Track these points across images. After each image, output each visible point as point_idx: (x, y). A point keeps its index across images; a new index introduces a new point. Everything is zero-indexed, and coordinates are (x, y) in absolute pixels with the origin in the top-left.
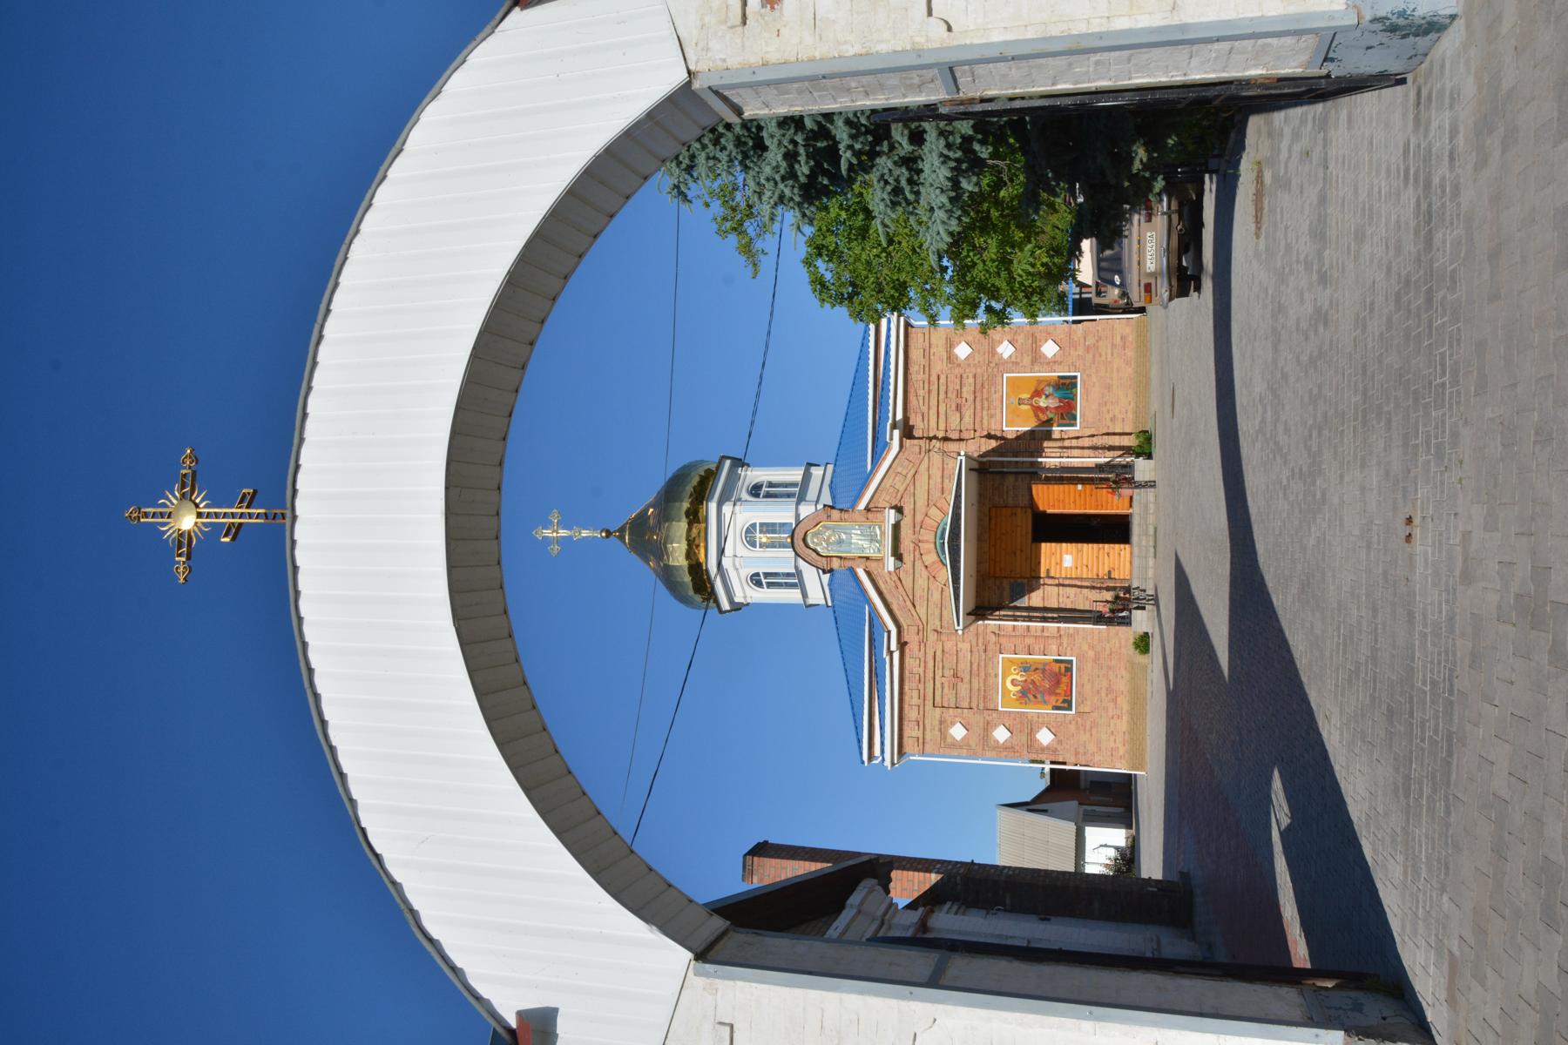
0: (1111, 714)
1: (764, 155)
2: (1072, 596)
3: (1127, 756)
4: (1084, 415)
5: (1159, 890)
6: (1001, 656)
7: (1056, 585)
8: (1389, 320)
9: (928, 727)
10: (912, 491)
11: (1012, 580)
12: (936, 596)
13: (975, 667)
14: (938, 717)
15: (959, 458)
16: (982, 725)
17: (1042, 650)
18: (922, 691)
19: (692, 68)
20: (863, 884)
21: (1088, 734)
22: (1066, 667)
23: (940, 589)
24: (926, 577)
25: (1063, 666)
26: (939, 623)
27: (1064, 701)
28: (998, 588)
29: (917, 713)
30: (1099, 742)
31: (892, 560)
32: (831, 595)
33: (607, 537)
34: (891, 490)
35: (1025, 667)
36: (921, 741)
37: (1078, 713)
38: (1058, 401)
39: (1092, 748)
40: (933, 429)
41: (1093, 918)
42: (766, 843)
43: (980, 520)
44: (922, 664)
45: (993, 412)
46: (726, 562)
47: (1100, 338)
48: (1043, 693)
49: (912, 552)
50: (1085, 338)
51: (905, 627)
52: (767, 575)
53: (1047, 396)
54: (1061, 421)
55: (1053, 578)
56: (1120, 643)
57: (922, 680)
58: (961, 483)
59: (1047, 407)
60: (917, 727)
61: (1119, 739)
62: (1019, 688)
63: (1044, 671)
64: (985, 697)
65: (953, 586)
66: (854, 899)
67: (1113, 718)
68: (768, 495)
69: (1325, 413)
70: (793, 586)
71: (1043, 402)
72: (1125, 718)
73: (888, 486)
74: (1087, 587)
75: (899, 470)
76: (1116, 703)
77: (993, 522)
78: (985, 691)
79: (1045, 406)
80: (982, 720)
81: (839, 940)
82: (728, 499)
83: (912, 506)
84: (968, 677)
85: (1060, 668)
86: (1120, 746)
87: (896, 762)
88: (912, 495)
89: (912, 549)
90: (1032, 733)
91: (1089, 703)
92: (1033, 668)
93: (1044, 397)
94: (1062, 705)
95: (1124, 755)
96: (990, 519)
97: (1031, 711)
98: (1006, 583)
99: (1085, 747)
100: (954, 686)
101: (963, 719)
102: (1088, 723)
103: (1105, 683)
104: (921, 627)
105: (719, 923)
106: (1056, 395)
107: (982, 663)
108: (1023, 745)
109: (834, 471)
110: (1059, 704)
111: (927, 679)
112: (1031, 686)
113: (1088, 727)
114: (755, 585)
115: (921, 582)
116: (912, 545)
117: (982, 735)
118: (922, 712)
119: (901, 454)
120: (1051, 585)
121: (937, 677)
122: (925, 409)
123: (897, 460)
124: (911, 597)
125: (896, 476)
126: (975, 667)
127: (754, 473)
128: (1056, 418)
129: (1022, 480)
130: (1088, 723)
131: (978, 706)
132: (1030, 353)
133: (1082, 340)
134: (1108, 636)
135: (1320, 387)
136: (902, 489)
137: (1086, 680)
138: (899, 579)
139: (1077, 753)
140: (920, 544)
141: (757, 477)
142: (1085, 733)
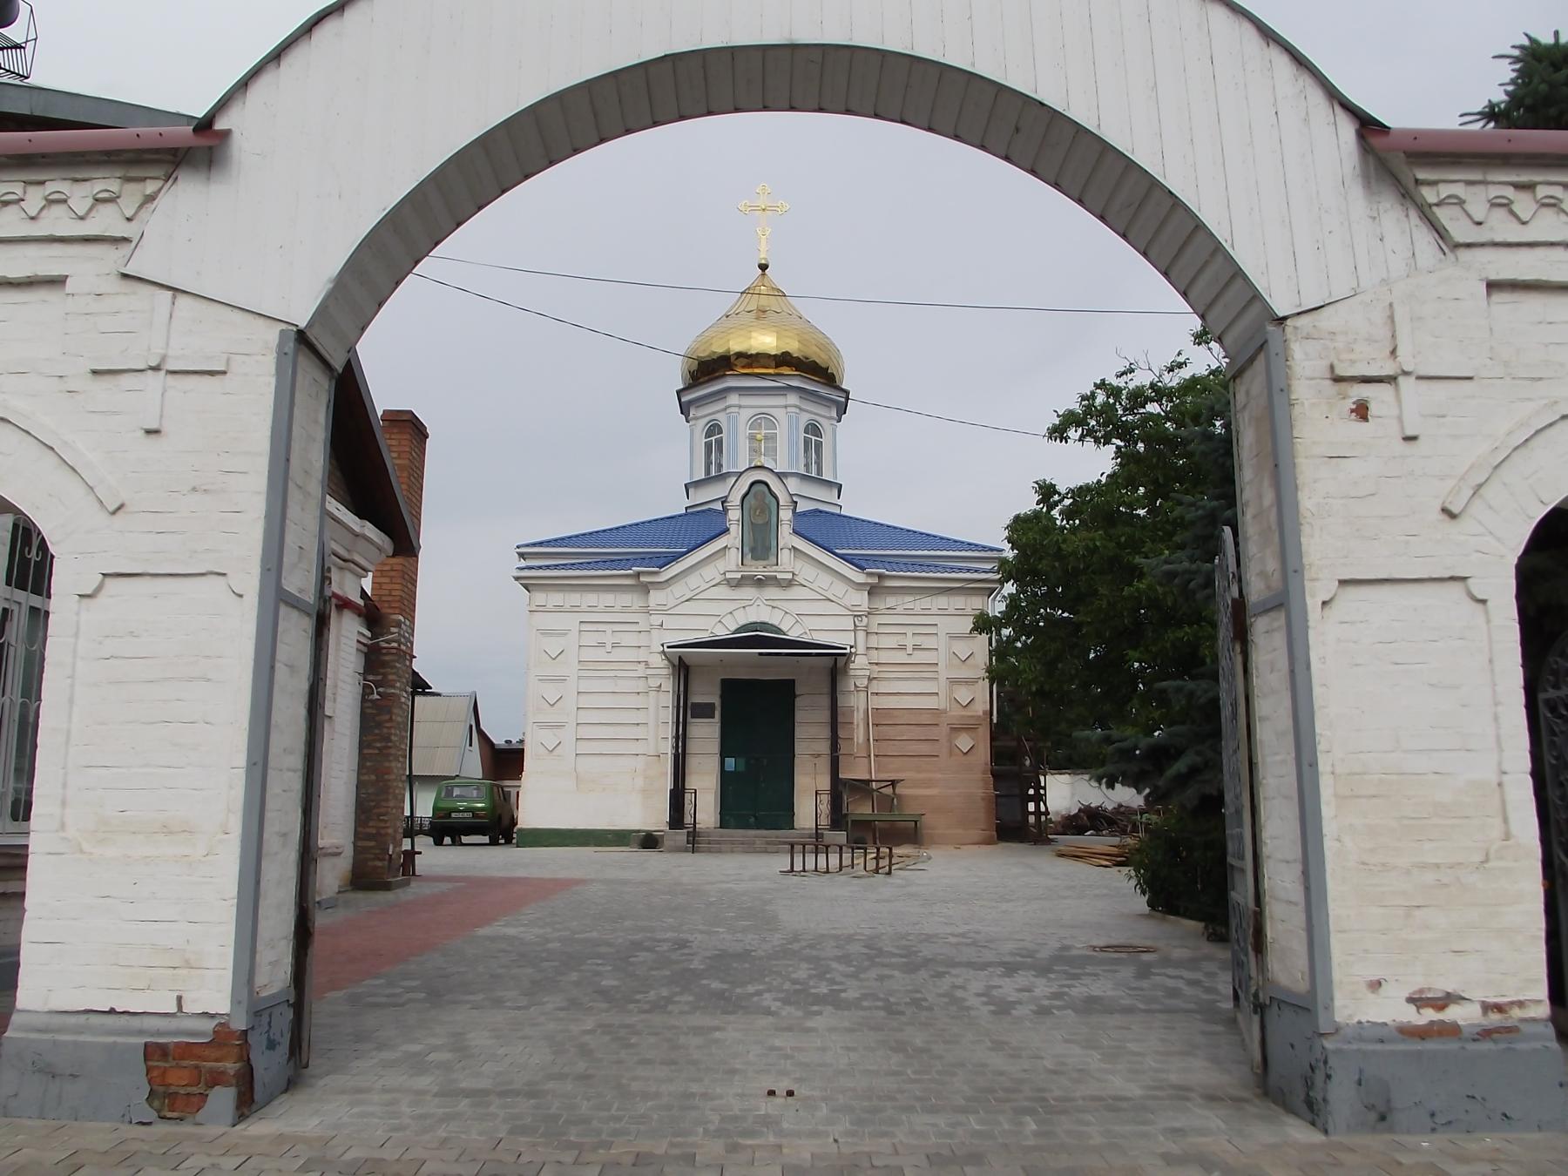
1: (1206, 373)
5: (391, 856)
8: (1001, 1073)
15: (848, 647)
19: (1289, 322)
20: (387, 539)
32: (698, 512)
41: (359, 774)
42: (426, 436)
52: (720, 442)
66: (370, 530)
68: (807, 442)
69: (902, 1013)
81: (325, 513)
105: (339, 366)
109: (833, 514)
135: (930, 1009)
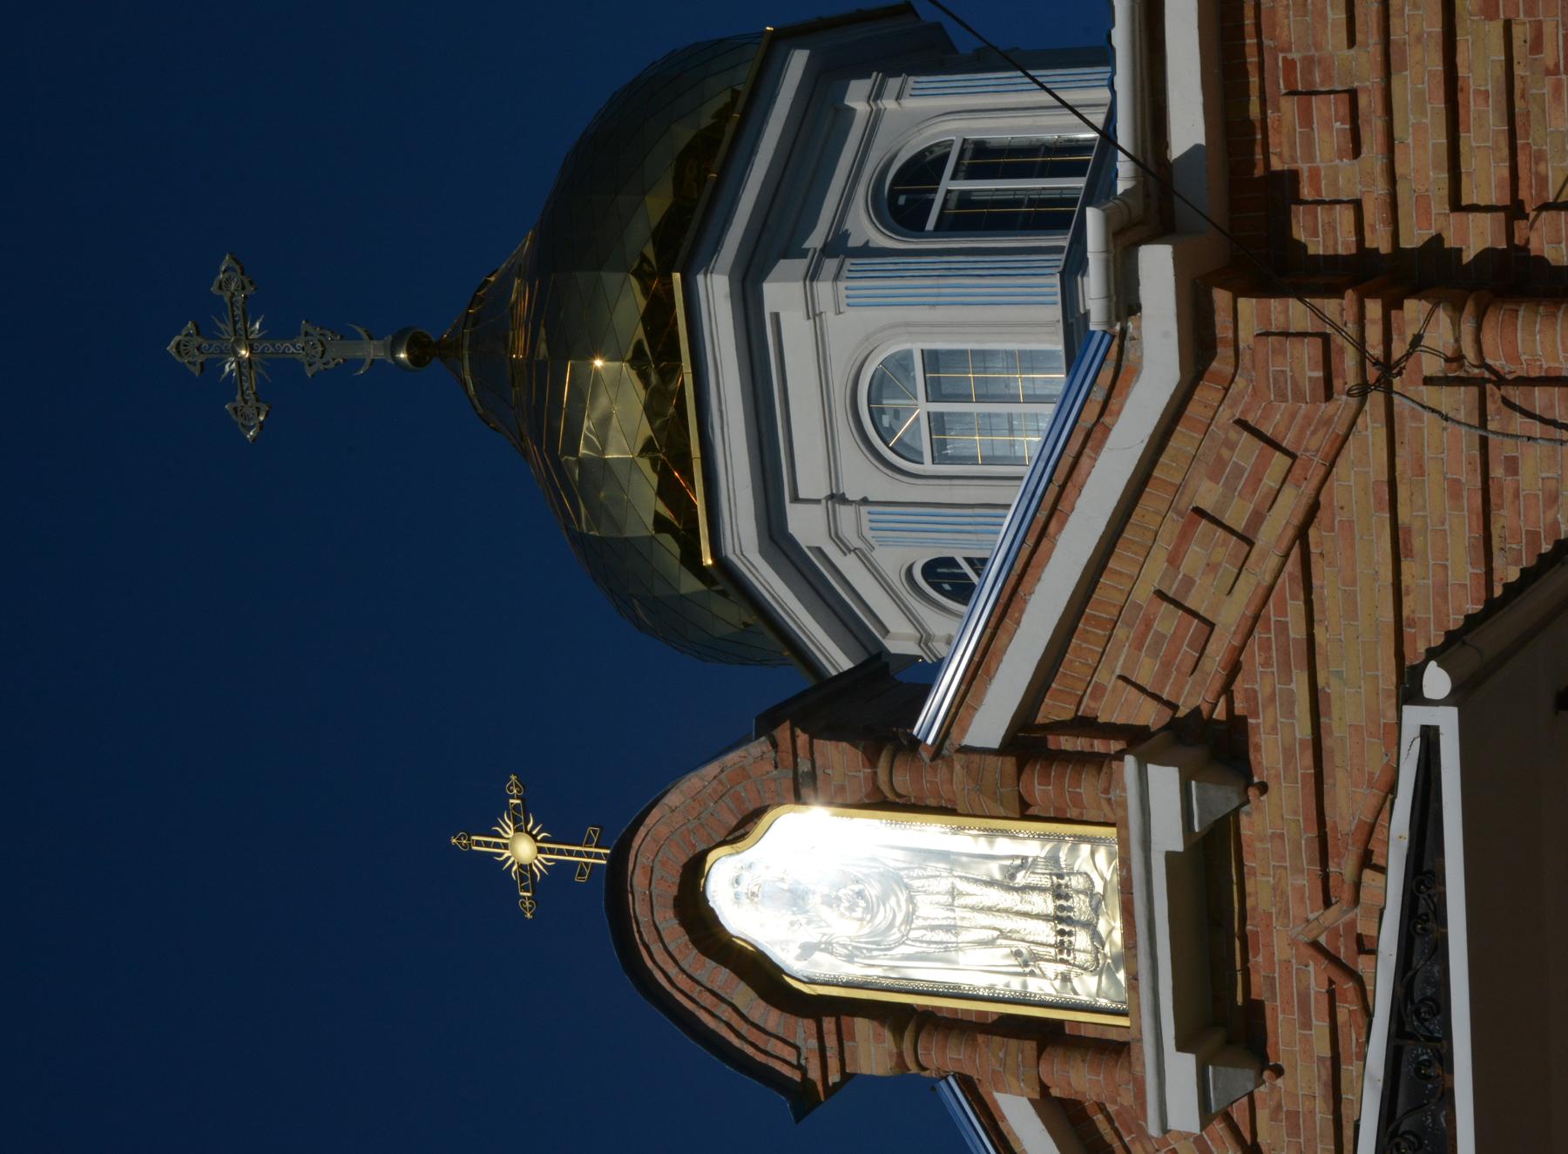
10: (1297, 631)
15: (1414, 717)
34: (1167, 621)
40: (1423, 201)
46: (805, 525)
49: (1318, 1006)
58: (1438, 877)
73: (1143, 593)
75: (1207, 494)
82: (793, 250)
83: (1303, 730)
88: (1297, 654)
116: (1315, 976)
119: (1206, 394)
122: (1362, 66)
123: (1182, 441)
125: (1184, 537)
127: (909, 103)
136: (1230, 615)
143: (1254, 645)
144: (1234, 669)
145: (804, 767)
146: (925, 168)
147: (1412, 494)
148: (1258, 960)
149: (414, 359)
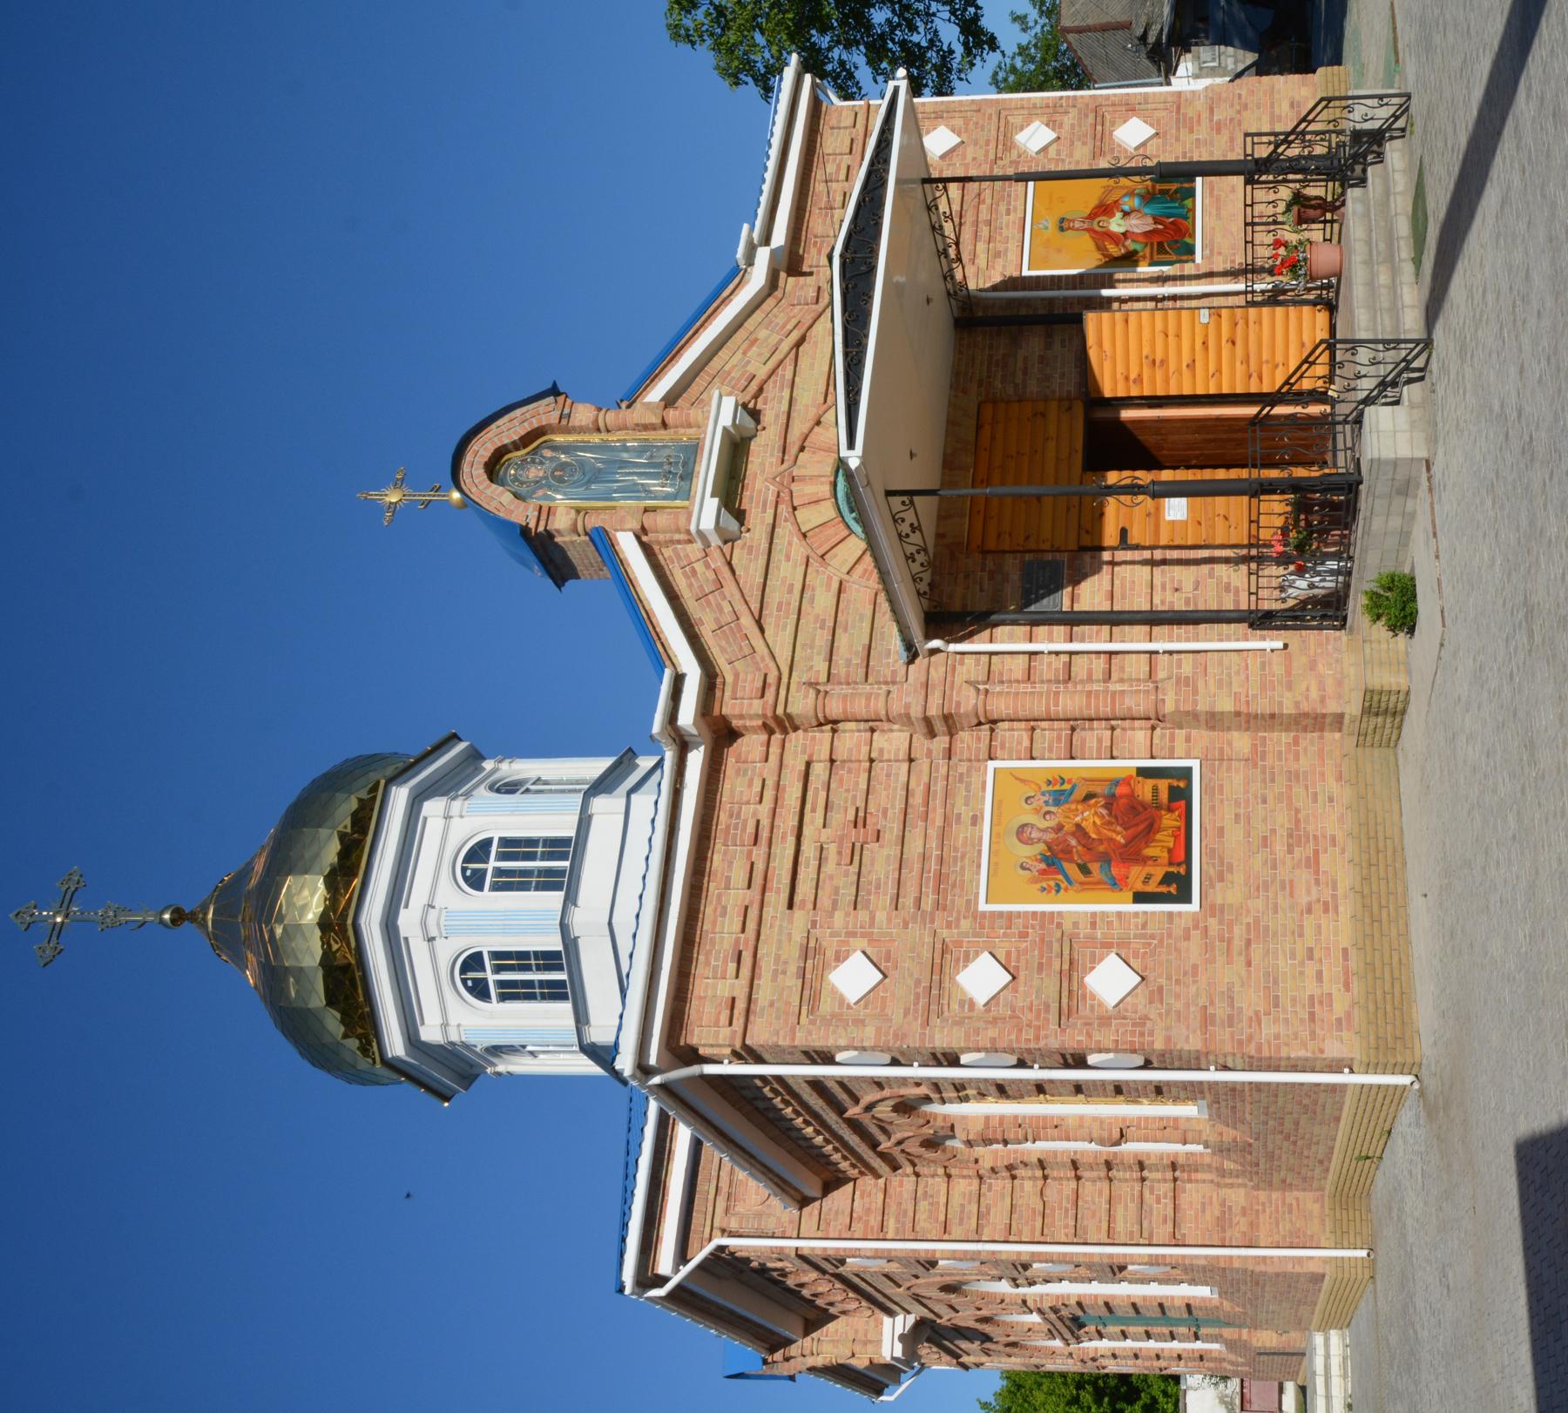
0: (1304, 900)
2: (1188, 586)
3: (1356, 1013)
4: (1212, 241)
6: (991, 765)
7: (1144, 562)
9: (766, 966)
11: (1028, 557)
12: (823, 601)
13: (917, 799)
14: (798, 937)
16: (926, 954)
17: (1107, 743)
18: (760, 867)
21: (1240, 961)
22: (1171, 788)
23: (835, 585)
24: (801, 560)
25: (1163, 785)
26: (823, 667)
27: (1168, 879)
28: (991, 578)
29: (737, 926)
30: (1272, 979)
31: (712, 505)
33: (174, 921)
35: (1060, 792)
36: (741, 1005)
37: (1209, 908)
38: (1150, 220)
39: (1250, 1000)
43: (952, 424)
44: (769, 794)
45: (1001, 247)
46: (408, 922)
47: (1246, 107)
48: (1106, 859)
50: (1212, 111)
51: (729, 678)
52: (504, 959)
53: (1126, 214)
54: (1156, 257)
55: (1137, 547)
56: (1321, 687)
57: (764, 834)
59: (1125, 234)
60: (732, 966)
61: (1332, 969)
62: (1041, 847)
63: (1110, 802)
64: (940, 878)
65: (846, 355)
67: (1309, 911)
70: (554, 992)
71: (1116, 225)
72: (1346, 909)
74: (1227, 561)
76: (1317, 872)
77: (987, 431)
78: (941, 860)
79: (1122, 230)
80: (928, 939)
84: (896, 827)
85: (1155, 790)
86: (1336, 990)
87: (653, 1061)
88: (787, 383)
89: (771, 498)
90: (1072, 972)
91: (1238, 877)
92: (1080, 793)
93: (1119, 215)
94: (1163, 889)
95: (1349, 1015)
96: (979, 427)
97: (1075, 908)
98: (1012, 565)
99: (1231, 999)
100: (855, 854)
101: (871, 941)
102: (1238, 931)
103: (1282, 819)
104: (772, 679)
106: (1147, 210)
107: (939, 787)
108: (1047, 1006)
110: (1152, 887)
111: (778, 833)
112: (1073, 842)
113: (1238, 943)
114: (470, 990)
115: (787, 571)
117: (925, 984)
118: (751, 925)
120: (1133, 563)
121: (806, 831)
124: (755, 606)
126: (917, 799)
128: (1148, 251)
129: (1063, 341)
130: (1238, 931)
131: (918, 901)
132: (1090, 141)
133: (1205, 115)
134: (1288, 673)
137: (1229, 817)
138: (729, 564)
139: (1207, 1020)
140: (794, 487)
141: (518, 772)
142: (1230, 962)
143: (771, 381)
144: (761, 390)
145: (566, 411)
146: (480, 851)
147: (818, 423)
148: (746, 494)
149: (173, 921)
